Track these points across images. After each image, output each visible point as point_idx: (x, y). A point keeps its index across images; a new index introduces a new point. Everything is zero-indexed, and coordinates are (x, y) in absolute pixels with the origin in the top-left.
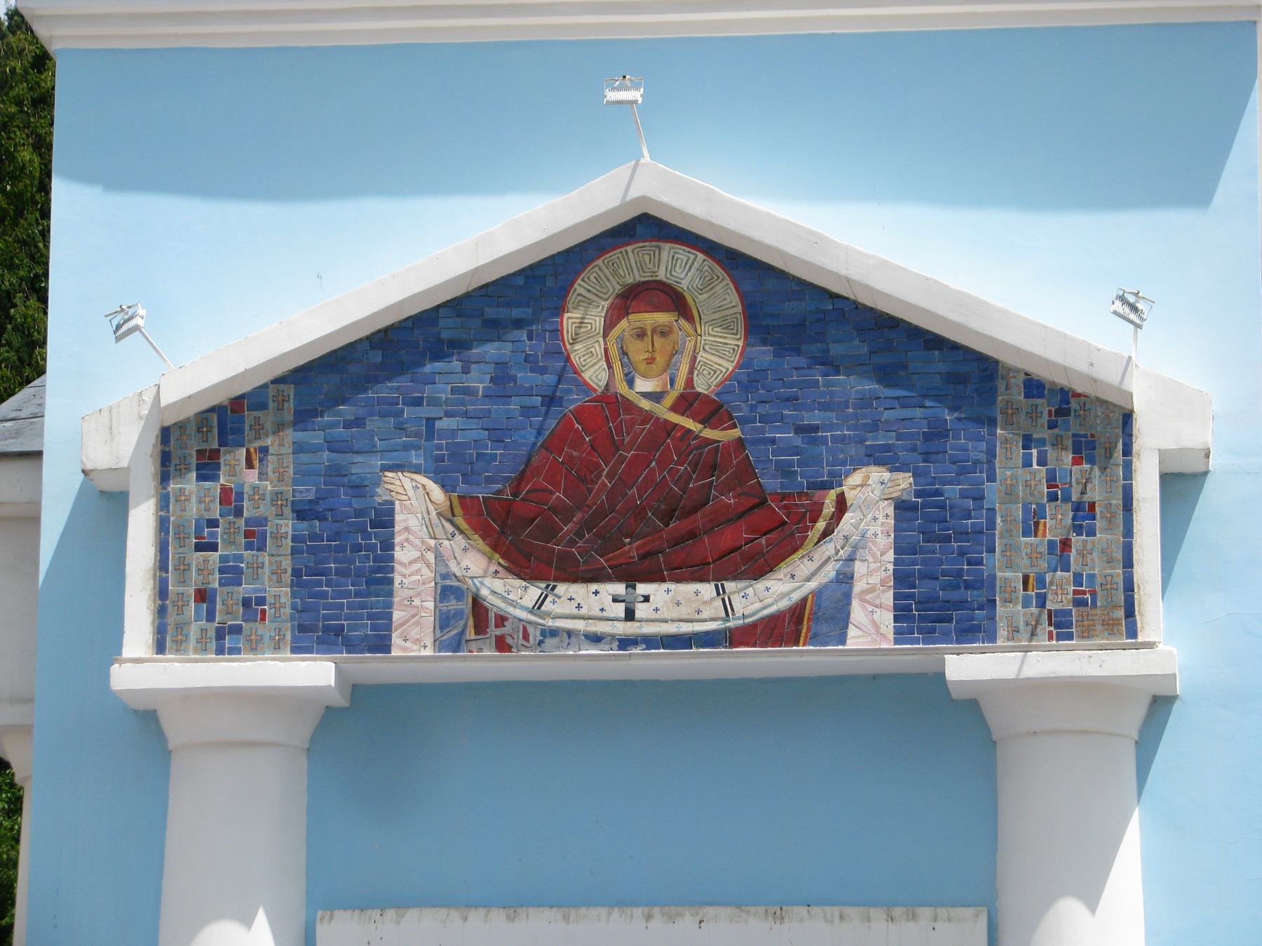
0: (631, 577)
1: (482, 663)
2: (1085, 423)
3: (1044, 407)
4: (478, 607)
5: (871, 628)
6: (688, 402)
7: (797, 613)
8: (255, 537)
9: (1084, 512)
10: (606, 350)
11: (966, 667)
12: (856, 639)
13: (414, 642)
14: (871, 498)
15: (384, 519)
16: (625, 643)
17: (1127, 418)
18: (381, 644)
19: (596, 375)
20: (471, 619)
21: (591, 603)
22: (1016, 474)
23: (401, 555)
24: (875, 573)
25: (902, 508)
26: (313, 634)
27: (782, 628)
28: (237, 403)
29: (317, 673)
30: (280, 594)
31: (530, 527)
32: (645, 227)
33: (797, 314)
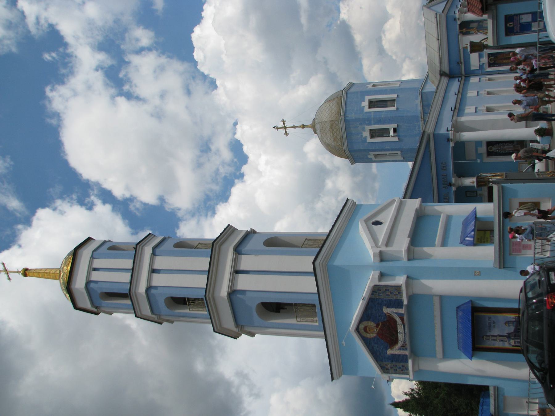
0: (397, 333)
1: (408, 346)
2: (376, 290)
3: (374, 293)
4: (402, 346)
5: (402, 311)
6: (377, 326)
7: (400, 318)
8: (395, 366)
9: (386, 290)
10: (404, 338)
11: (405, 302)
12: (403, 312)
13: (406, 352)
14: (386, 310)
15: (392, 355)
16: (405, 333)
17: (375, 285)
18: (407, 356)
19: (375, 335)
20: (403, 347)
21: (400, 336)
22: (383, 296)
23: (396, 353)
24: (395, 310)
25: (387, 307)
26: (406, 361)
27: (402, 320)
28: (381, 367)
29: (410, 361)
30: (401, 364)
31: (393, 341)
32: (357, 330)
33: (366, 316)
